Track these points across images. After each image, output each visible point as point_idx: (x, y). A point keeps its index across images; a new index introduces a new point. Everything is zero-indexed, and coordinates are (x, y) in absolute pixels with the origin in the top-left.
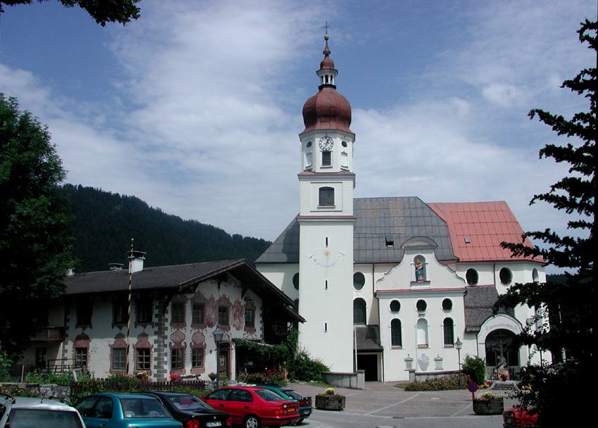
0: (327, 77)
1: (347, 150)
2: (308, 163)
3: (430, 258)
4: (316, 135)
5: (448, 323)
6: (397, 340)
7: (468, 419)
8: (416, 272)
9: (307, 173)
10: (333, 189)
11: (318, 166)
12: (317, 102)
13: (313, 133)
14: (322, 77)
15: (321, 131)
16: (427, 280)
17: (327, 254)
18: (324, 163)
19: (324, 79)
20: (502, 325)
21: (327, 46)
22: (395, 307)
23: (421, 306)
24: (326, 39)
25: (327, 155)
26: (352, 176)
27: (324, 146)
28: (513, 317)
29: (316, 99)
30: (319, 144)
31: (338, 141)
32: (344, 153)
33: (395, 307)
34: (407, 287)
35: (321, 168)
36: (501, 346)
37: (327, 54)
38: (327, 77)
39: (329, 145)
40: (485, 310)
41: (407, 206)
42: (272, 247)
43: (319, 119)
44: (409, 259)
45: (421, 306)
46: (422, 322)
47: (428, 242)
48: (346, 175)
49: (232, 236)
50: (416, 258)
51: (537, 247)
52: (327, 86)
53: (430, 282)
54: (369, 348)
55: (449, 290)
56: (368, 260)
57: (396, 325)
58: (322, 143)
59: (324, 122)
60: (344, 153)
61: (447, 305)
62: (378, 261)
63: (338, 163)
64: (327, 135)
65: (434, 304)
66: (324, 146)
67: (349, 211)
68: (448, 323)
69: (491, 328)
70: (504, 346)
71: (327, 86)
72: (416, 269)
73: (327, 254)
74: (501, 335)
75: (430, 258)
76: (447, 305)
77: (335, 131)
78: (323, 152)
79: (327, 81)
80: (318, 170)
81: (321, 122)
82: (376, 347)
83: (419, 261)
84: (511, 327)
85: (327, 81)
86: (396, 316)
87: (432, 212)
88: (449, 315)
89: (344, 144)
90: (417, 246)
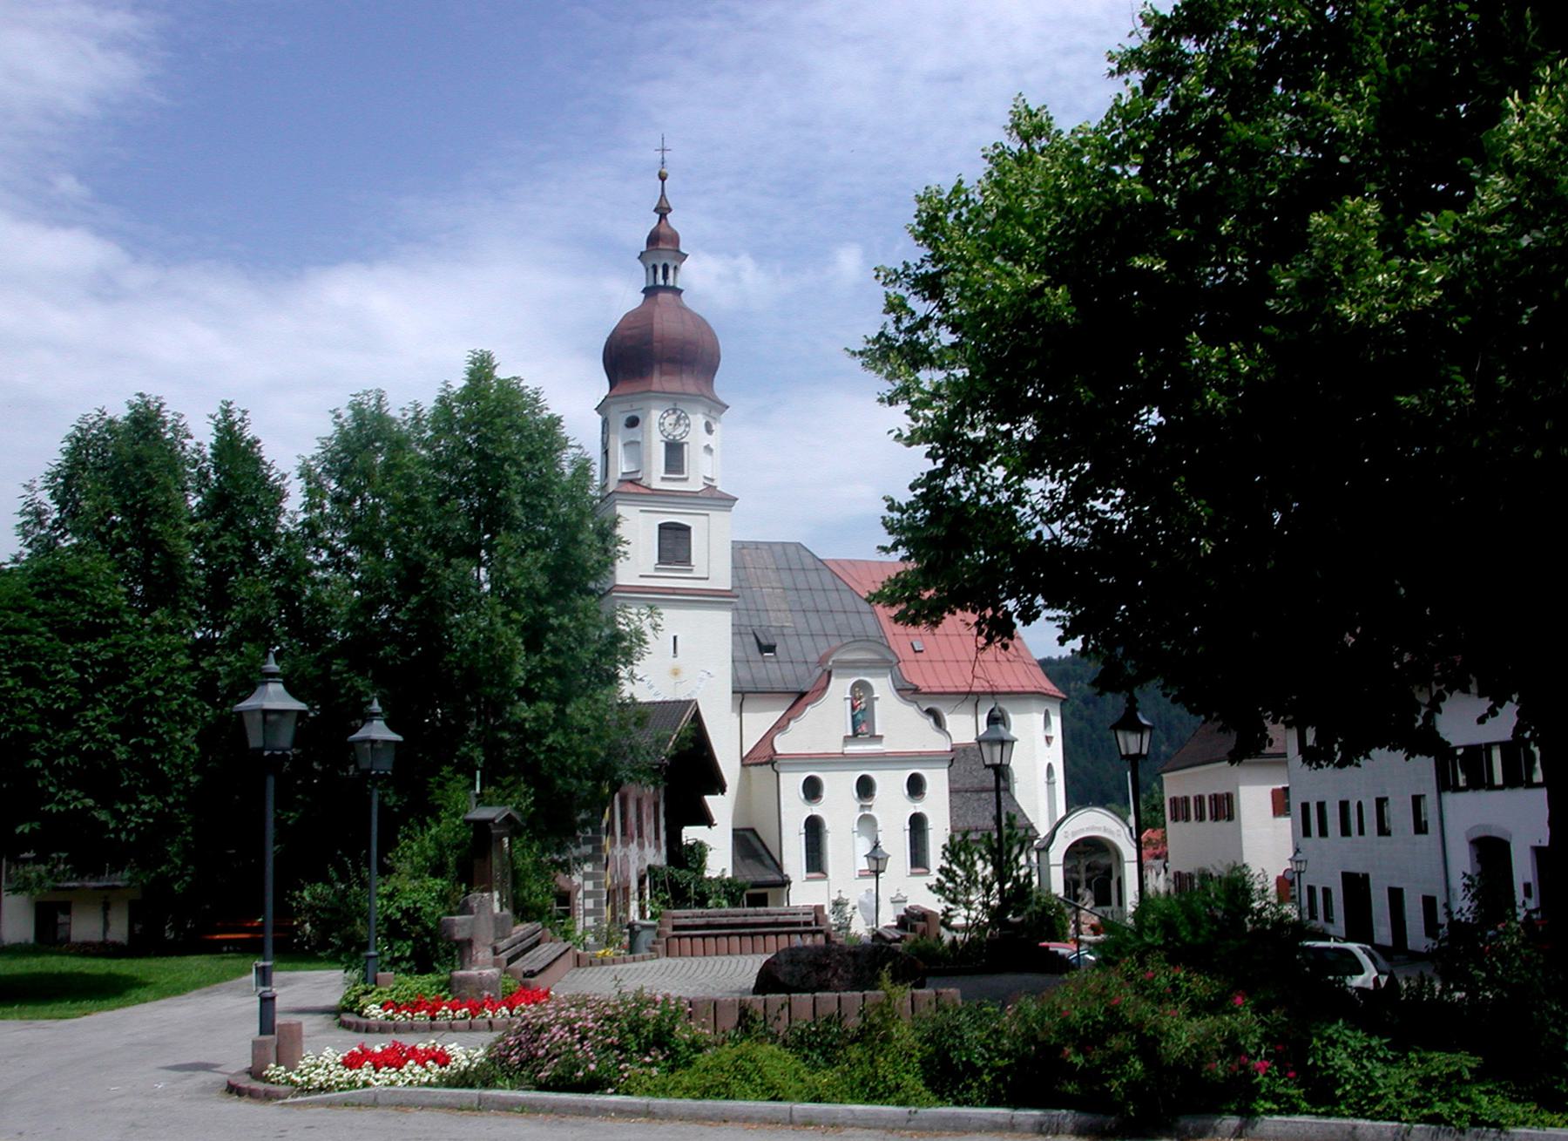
3: (882, 686)
4: (654, 403)
5: (918, 824)
6: (815, 861)
7: (1336, 949)
8: (853, 717)
9: (631, 488)
10: (687, 529)
11: (656, 476)
13: (649, 399)
14: (655, 268)
15: (665, 395)
16: (878, 733)
17: (676, 673)
18: (668, 469)
19: (660, 271)
20: (1093, 828)
21: (663, 194)
22: (812, 789)
23: (865, 788)
25: (674, 452)
27: (669, 429)
32: (708, 449)
33: (812, 789)
34: (836, 746)
35: (663, 479)
36: (1082, 869)
37: (663, 211)
39: (680, 430)
40: (975, 796)
41: (784, 565)
42: (1224, 752)
43: (657, 367)
44: (840, 687)
45: (865, 788)
46: (867, 822)
47: (875, 652)
50: (854, 686)
51: (69, 438)
53: (881, 737)
55: (920, 754)
56: (779, 686)
57: (814, 828)
61: (916, 786)
62: (750, 687)
63: (700, 469)
65: (892, 784)
67: (722, 579)
68: (918, 824)
69: (1074, 834)
70: (1088, 868)
72: (853, 708)
73: (676, 673)
74: (1081, 848)
75: (882, 686)
76: (916, 786)
77: (694, 399)
78: (667, 444)
79: (665, 277)
80: (657, 484)
81: (662, 373)
84: (1111, 832)
87: (838, 581)
88: (919, 807)
89: (709, 430)
90: (854, 662)
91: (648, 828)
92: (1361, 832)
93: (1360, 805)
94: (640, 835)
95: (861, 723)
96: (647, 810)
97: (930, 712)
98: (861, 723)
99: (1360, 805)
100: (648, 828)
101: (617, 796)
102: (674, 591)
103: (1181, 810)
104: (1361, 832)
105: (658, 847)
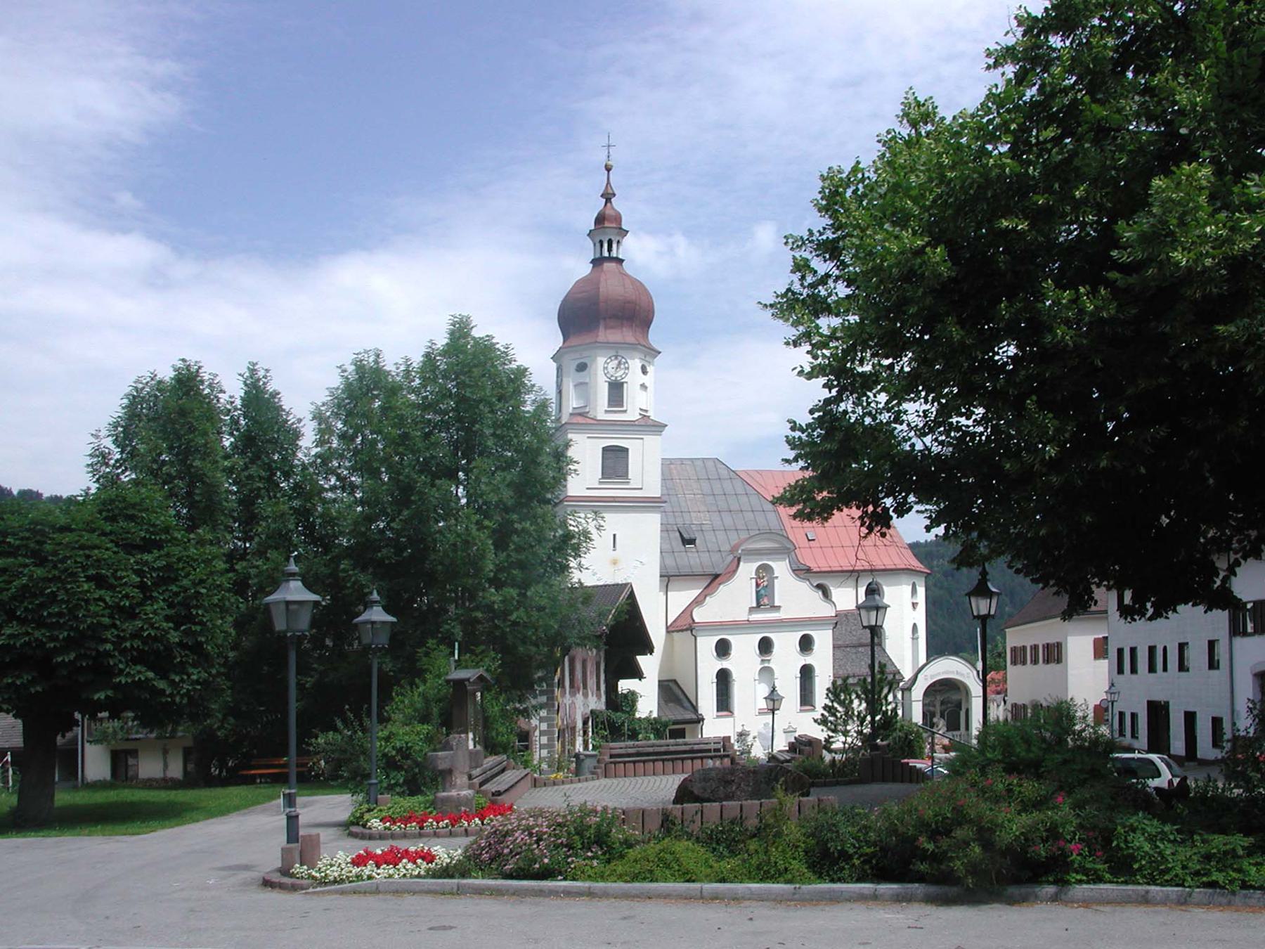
0: (610, 243)
1: (646, 380)
2: (579, 397)
3: (781, 568)
5: (807, 673)
6: (724, 702)
8: (757, 592)
12: (602, 285)
14: (601, 243)
15: (608, 345)
17: (615, 562)
19: (606, 246)
22: (723, 649)
23: (765, 646)
24: (608, 169)
25: (616, 389)
26: (658, 428)
27: (612, 371)
28: (929, 661)
29: (598, 283)
30: (602, 368)
31: (635, 364)
32: (644, 387)
33: (723, 649)
34: (743, 616)
35: (606, 412)
37: (608, 197)
38: (610, 243)
43: (602, 323)
44: (747, 570)
45: (765, 646)
48: (648, 426)
49: (15, 492)
52: (611, 259)
54: (679, 717)
56: (698, 570)
57: (724, 678)
58: (610, 366)
59: (612, 328)
60: (644, 387)
61: (806, 644)
63: (637, 402)
64: (618, 351)
65: (786, 643)
66: (612, 371)
67: (654, 489)
68: (807, 673)
69: (932, 677)
71: (611, 259)
72: (758, 585)
73: (615, 562)
75: (781, 568)
76: (806, 644)
77: (633, 347)
79: (610, 250)
80: (601, 416)
81: (606, 328)
82: (694, 717)
83: (765, 572)
85: (610, 250)
86: (725, 664)
89: (644, 371)
91: (591, 682)
92: (1165, 669)
93: (1165, 649)
94: (585, 687)
95: (764, 596)
96: (591, 668)
97: (819, 587)
98: (764, 596)
99: (1165, 649)
100: (591, 682)
101: (566, 659)
102: (614, 499)
103: (1019, 656)
104: (1165, 669)
105: (599, 697)
